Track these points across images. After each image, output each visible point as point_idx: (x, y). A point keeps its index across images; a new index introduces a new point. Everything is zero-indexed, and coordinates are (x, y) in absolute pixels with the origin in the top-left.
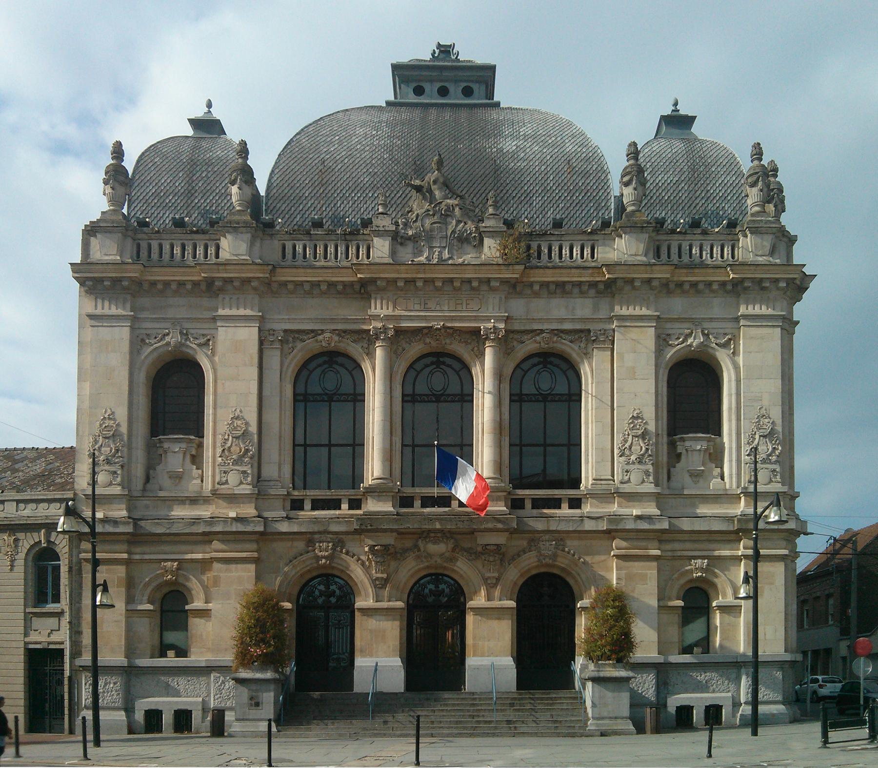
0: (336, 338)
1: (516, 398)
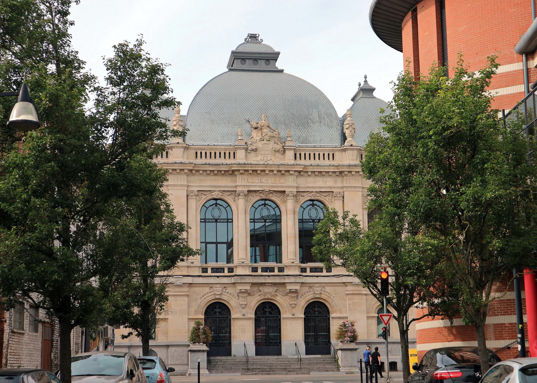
0: (221, 194)
1: (203, 220)
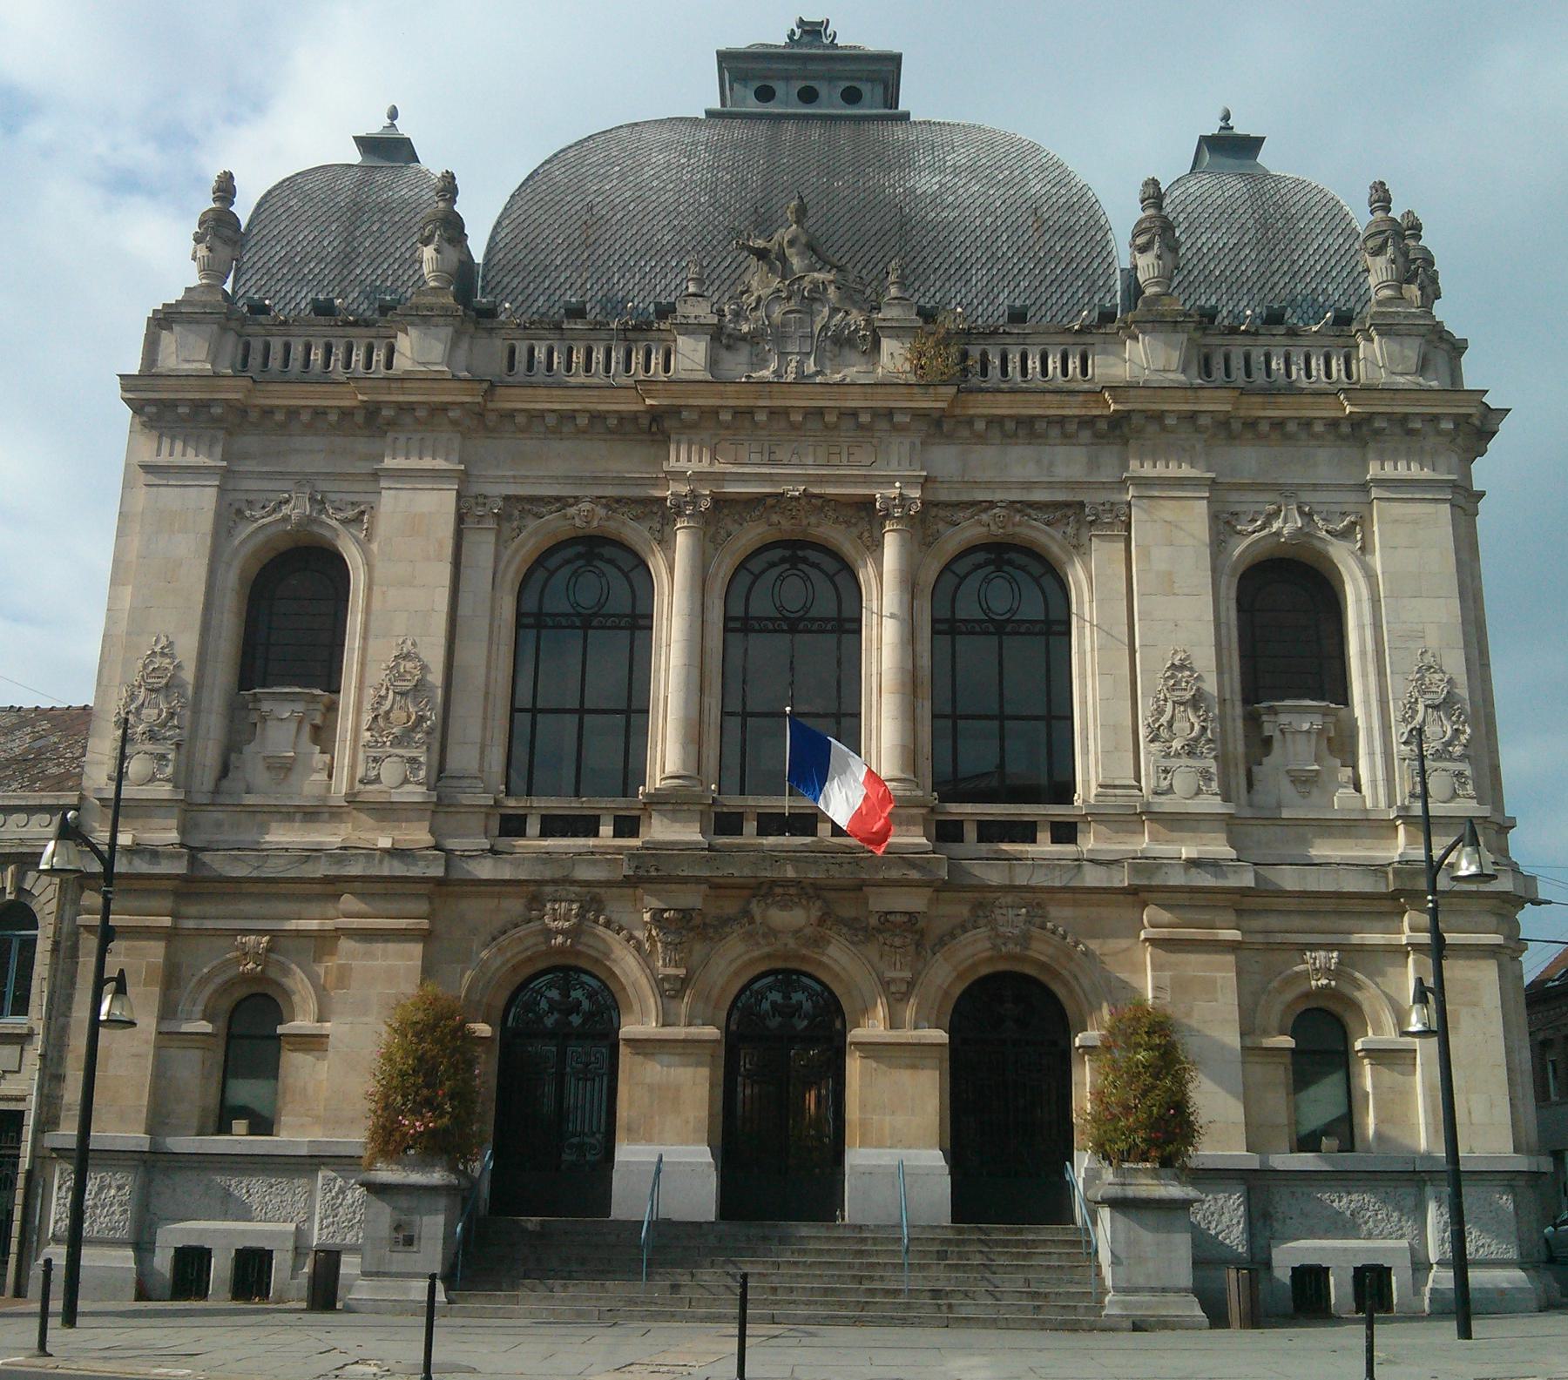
0: (601, 512)
